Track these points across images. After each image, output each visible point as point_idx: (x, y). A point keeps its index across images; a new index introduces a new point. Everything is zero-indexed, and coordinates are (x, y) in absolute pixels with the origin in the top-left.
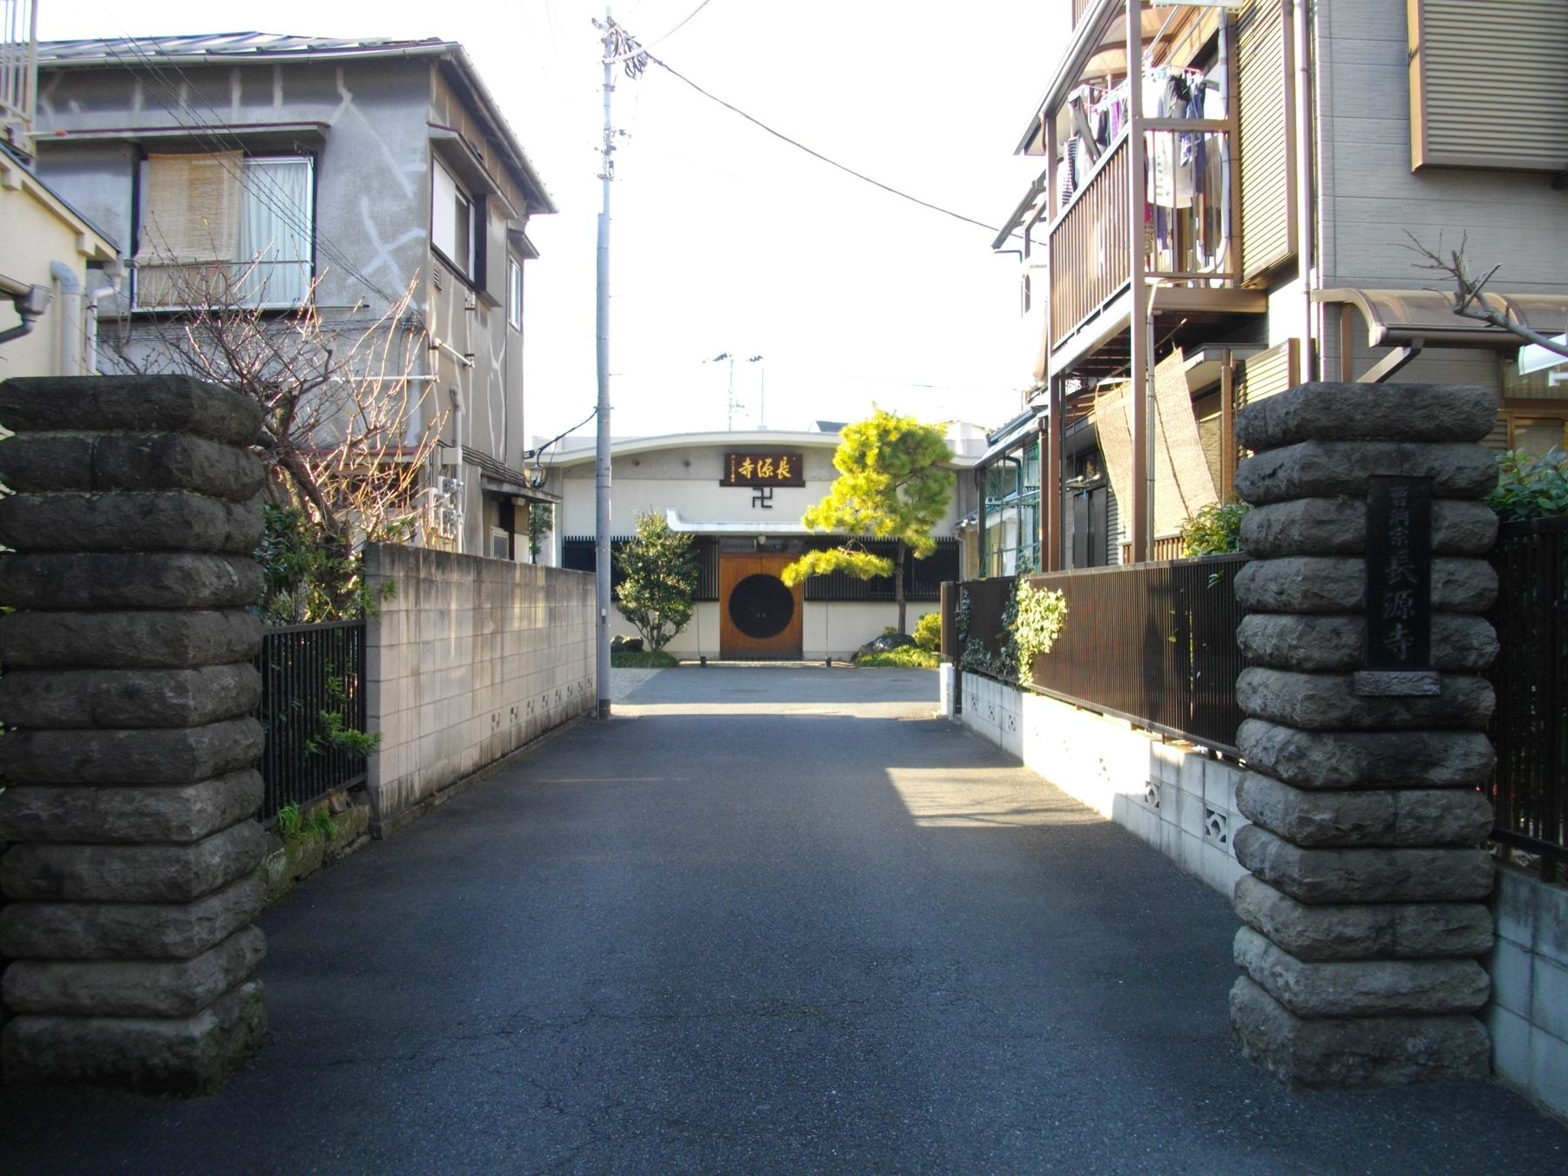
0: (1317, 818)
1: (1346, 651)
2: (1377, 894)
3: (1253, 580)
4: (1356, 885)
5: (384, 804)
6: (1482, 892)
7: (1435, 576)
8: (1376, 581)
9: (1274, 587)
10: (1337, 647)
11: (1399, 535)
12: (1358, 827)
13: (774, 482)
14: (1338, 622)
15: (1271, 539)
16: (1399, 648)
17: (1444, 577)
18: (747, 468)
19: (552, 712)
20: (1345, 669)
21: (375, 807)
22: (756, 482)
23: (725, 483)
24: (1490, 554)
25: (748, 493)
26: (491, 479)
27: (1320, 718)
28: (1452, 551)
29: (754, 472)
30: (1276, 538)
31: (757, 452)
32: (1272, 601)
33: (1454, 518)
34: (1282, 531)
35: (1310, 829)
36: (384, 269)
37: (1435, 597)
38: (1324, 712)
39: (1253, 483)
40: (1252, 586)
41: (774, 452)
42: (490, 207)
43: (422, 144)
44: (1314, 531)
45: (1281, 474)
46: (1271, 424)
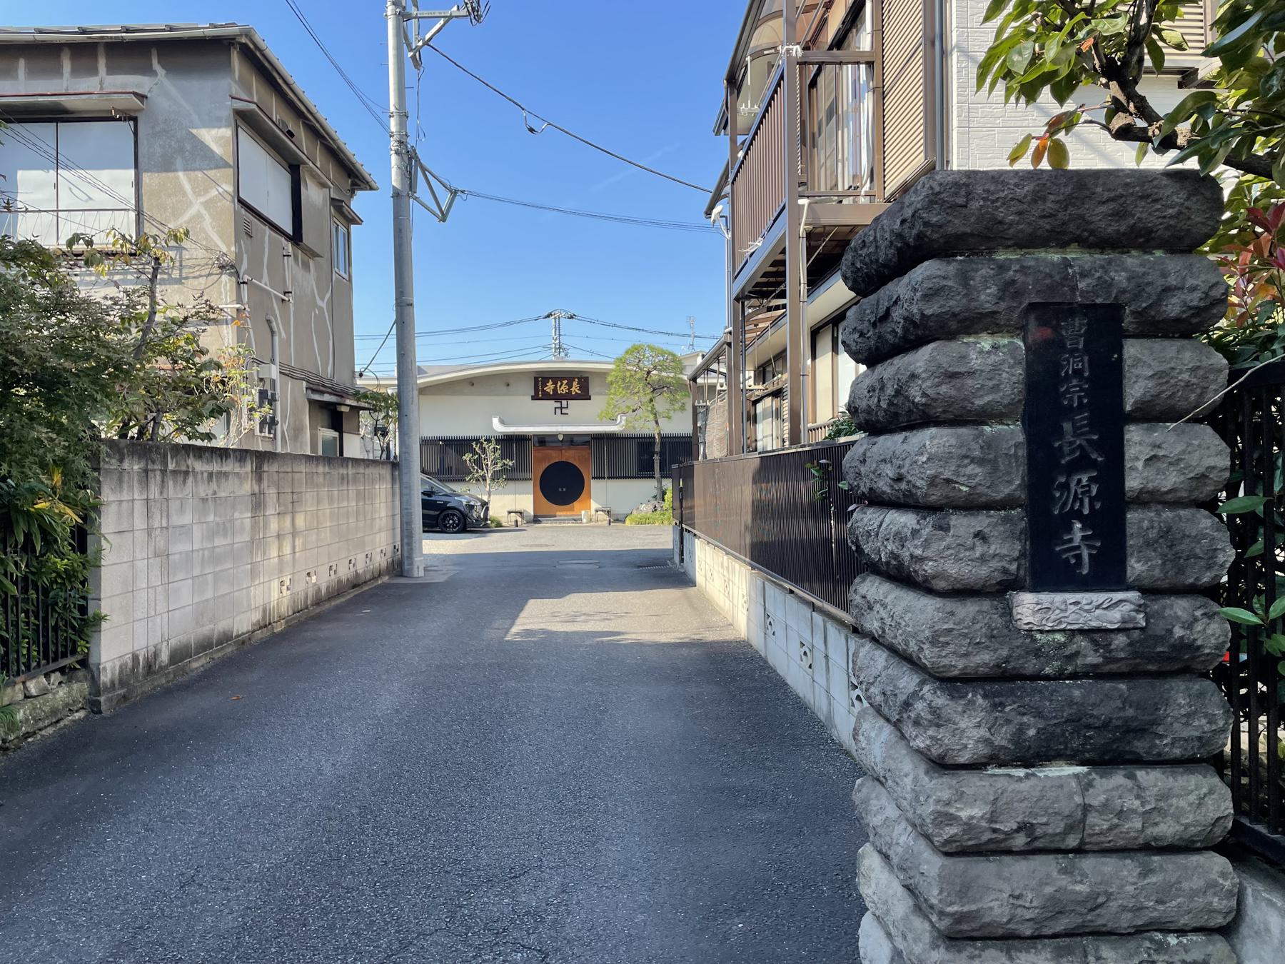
0: (964, 814)
1: (995, 564)
2: (1061, 925)
3: (863, 462)
4: (1029, 915)
5: (105, 678)
6: (1219, 920)
7: (1130, 452)
8: (1043, 464)
9: (889, 471)
10: (983, 559)
11: (1074, 393)
12: (1023, 827)
13: (569, 397)
14: (981, 522)
15: (884, 405)
16: (1079, 557)
17: (1148, 453)
18: (550, 387)
19: (360, 571)
20: (1001, 590)
21: (94, 680)
22: (556, 397)
23: (534, 398)
24: (1223, 419)
25: (552, 404)
26: (314, 391)
27: (961, 664)
28: (1154, 413)
29: (555, 390)
30: (891, 404)
31: (557, 376)
32: (888, 490)
33: (1145, 366)
34: (898, 393)
35: (952, 831)
36: (198, 216)
37: (1132, 483)
38: (966, 655)
39: (862, 334)
40: (863, 470)
41: (569, 376)
42: (303, 173)
43: (227, 113)
44: (944, 389)
45: (897, 314)
46: (883, 244)
